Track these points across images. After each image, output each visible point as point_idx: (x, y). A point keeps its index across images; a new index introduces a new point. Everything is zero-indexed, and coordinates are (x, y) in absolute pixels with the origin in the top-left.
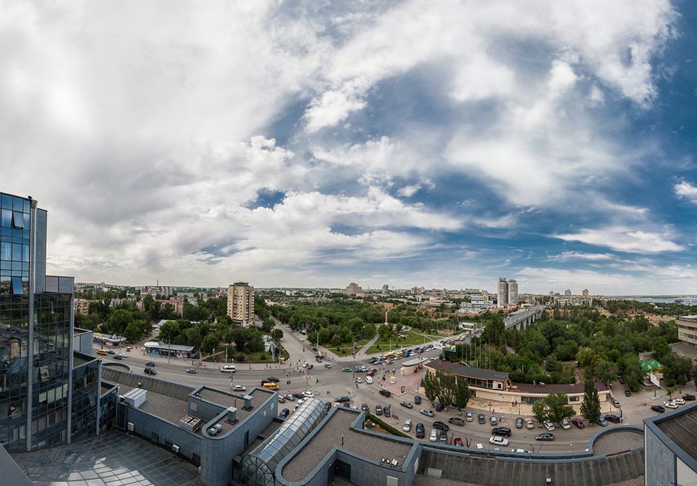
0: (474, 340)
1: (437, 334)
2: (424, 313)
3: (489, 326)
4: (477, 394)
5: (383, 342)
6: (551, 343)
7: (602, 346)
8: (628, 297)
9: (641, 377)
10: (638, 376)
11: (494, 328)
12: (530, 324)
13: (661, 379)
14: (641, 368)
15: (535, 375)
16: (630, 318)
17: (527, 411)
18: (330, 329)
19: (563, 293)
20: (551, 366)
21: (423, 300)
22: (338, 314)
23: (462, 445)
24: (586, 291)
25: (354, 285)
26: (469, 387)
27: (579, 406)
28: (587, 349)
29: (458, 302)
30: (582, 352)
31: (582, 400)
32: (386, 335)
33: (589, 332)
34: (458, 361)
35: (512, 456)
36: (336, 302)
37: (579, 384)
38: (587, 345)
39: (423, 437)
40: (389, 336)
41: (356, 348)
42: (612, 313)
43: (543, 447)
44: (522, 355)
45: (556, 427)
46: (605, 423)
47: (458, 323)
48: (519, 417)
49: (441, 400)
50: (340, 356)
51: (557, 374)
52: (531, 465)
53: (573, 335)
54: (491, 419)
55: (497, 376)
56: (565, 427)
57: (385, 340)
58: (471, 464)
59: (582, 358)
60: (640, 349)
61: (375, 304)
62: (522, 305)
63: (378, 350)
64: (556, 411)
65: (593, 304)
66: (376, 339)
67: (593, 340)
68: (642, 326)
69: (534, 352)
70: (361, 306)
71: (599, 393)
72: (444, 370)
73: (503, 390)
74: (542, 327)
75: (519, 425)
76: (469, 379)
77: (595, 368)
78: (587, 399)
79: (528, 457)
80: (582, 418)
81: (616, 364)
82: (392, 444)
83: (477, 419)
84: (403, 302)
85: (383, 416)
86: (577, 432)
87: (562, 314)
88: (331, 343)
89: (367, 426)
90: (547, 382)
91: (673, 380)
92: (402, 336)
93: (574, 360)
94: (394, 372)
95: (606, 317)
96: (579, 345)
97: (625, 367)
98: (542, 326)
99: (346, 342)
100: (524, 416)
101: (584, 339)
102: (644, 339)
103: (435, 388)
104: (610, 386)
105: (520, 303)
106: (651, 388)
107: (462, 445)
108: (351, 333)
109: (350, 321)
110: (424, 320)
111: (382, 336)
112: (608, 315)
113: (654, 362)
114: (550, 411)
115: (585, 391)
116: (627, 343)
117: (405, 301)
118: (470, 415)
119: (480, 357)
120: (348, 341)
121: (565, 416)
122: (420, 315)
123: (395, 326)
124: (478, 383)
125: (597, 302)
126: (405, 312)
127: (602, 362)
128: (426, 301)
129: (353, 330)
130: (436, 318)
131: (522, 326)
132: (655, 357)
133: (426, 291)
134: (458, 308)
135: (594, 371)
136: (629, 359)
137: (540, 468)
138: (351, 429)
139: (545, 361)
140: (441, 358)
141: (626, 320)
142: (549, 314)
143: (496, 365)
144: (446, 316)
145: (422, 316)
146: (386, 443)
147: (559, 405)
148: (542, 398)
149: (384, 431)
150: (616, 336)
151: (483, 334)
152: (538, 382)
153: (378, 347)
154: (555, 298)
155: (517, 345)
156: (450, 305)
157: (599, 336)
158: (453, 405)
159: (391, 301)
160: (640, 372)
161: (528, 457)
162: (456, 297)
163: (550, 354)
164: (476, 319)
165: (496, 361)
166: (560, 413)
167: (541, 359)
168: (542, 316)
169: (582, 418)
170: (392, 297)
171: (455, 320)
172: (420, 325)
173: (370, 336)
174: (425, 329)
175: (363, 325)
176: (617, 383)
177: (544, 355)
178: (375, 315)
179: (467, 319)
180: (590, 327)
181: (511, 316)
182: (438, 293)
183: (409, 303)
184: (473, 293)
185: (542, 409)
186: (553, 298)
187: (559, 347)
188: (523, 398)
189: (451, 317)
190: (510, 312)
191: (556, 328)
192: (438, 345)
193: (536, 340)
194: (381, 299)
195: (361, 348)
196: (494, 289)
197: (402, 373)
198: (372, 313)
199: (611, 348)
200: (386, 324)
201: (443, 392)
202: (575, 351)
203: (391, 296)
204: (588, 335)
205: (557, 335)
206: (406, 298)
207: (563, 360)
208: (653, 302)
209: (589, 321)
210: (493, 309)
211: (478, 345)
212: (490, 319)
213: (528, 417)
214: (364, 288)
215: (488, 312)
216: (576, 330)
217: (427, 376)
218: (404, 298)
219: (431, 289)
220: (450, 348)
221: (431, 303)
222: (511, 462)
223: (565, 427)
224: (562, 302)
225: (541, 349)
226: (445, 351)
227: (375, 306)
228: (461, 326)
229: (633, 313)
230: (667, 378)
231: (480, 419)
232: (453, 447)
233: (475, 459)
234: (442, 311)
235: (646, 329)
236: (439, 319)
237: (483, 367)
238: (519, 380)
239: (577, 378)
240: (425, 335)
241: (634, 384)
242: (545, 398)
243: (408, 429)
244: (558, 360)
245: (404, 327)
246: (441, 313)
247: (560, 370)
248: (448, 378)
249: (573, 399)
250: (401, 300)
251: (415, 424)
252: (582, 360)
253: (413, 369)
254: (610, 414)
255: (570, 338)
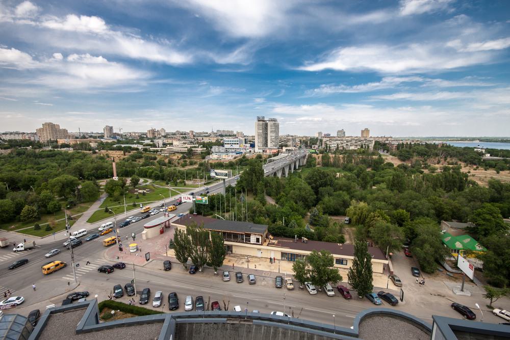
0: (229, 189)
1: (185, 185)
2: (167, 161)
3: (246, 173)
4: (234, 250)
5: (114, 203)
6: (317, 192)
7: (383, 203)
8: (434, 139)
9: (441, 256)
10: (436, 252)
11: (251, 174)
12: (292, 170)
13: (477, 269)
14: (443, 243)
15: (297, 229)
16: (433, 170)
17: (287, 269)
18: (13, 199)
19: (334, 134)
20: (315, 220)
21: (165, 145)
22: (26, 173)
23: (220, 309)
24: (366, 131)
25: (52, 127)
26: (226, 243)
27: (347, 272)
28: (362, 204)
29: (208, 146)
30: (355, 207)
31: (350, 265)
32: (116, 194)
33: (366, 183)
34: (211, 214)
35: (270, 320)
36: (19, 154)
37: (348, 245)
38: (362, 199)
39: (177, 308)
40: (122, 194)
41: (70, 218)
42: (403, 160)
43: (303, 312)
44: (282, 205)
45: (318, 291)
46: (378, 301)
47: (209, 171)
48: (278, 275)
49: (195, 260)
50: (42, 235)
51: (322, 229)
52: (290, 332)
53: (345, 186)
54: (249, 277)
55: (255, 229)
56: (329, 293)
57: (117, 200)
58: (229, 330)
59: (355, 214)
60: (444, 215)
61: (95, 153)
62: (284, 149)
63: (107, 214)
64: (319, 272)
65: (375, 148)
66: (102, 200)
67: (372, 193)
68: (455, 183)
69: (296, 203)
70: (69, 158)
71: (373, 260)
72: (196, 226)
73: (262, 245)
74: (307, 174)
75: (279, 284)
76: (224, 233)
77: (371, 229)
78: (357, 264)
79: (286, 322)
80: (349, 287)
81: (401, 229)
82: (138, 328)
83: (234, 278)
84: (137, 149)
85: (126, 296)
86: (341, 301)
87: (332, 160)
88: (20, 221)
89: (103, 318)
90: (311, 237)
91: (502, 278)
92: (140, 191)
93: (344, 214)
94: (134, 238)
95: (393, 165)
96: (351, 198)
97: (416, 235)
98: (306, 173)
99: (49, 213)
100: (284, 274)
101: (358, 190)
102: (455, 203)
103: (186, 248)
104: (390, 257)
105: (281, 146)
106: (456, 276)
107: (220, 309)
108: (57, 198)
109: (52, 181)
110: (167, 170)
111: (110, 195)
112: (396, 162)
113: (468, 240)
114: (313, 271)
115: (355, 255)
116: (424, 204)
117: (140, 147)
118: (226, 273)
119: (236, 208)
120: (57, 211)
121: (329, 280)
122: (162, 163)
123: (129, 181)
124: (235, 237)
125: (382, 145)
126: (142, 161)
127: (381, 223)
128: (168, 147)
129: (61, 193)
130: (183, 166)
131: (283, 173)
132: (473, 233)
133: (168, 134)
134: (209, 153)
135: (369, 232)
136: (424, 227)
137: (299, 337)
138: (79, 332)
139: (309, 214)
140: (192, 212)
141: (426, 171)
142: (315, 159)
143: (254, 216)
144: (195, 163)
145: (165, 165)
146: (132, 330)
147: (323, 265)
148: (304, 256)
149: (130, 315)
150: (406, 192)
151: (239, 183)
152: (300, 237)
153: (107, 211)
154: (324, 140)
155: (277, 195)
156: (199, 150)
157: (380, 189)
158: (208, 264)
159: (119, 149)
160: (439, 248)
161: (286, 322)
162: (206, 140)
163: (315, 205)
164: (231, 165)
165: (254, 212)
166: (322, 277)
167: (304, 211)
168: (307, 162)
169: (349, 287)
170: (122, 142)
171: (206, 168)
172: (163, 176)
173: (92, 197)
174: (169, 180)
175: (78, 184)
176: (401, 254)
177: (308, 207)
178: (97, 169)
179: (220, 165)
180: (368, 178)
181: (270, 161)
182: (184, 136)
183: (145, 150)
184: (226, 136)
185: (304, 268)
186: (321, 141)
187: (326, 199)
188: (283, 254)
189: (201, 165)
190: (270, 156)
191: (325, 175)
192: (187, 198)
193: (300, 189)
194: (102, 146)
195: (80, 216)
196: (251, 130)
197: (144, 237)
198: (90, 165)
199: (396, 206)
200: (116, 178)
201: (196, 251)
202: (346, 205)
203: (119, 142)
204: (364, 187)
205: (325, 185)
206: (141, 144)
207: (331, 214)
208: (481, 147)
209: (369, 170)
210: (251, 154)
211: (233, 195)
212: (246, 165)
213: (288, 275)
214: (72, 130)
215: (244, 157)
216: (348, 179)
217: (176, 235)
218: (138, 143)
219: (174, 131)
220: (202, 200)
221: (175, 149)
222: (268, 327)
223: (329, 293)
224: (333, 146)
225: (304, 200)
226: (196, 204)
227: (94, 156)
228: (213, 174)
229: (438, 163)
230: (490, 270)
231: (237, 277)
232: (210, 312)
233: (232, 324)
234: (189, 158)
235: (461, 188)
236: (187, 168)
237: (240, 220)
238: (280, 233)
239: (346, 237)
240: (170, 187)
241: (429, 261)
242: (307, 256)
243: (158, 303)
244: (324, 213)
245: (141, 180)
246: (188, 161)
247: (326, 226)
248: (201, 234)
249: (340, 261)
250: (135, 146)
251: (166, 295)
252: (355, 217)
253: (158, 229)
254: (387, 292)
255: (341, 189)
